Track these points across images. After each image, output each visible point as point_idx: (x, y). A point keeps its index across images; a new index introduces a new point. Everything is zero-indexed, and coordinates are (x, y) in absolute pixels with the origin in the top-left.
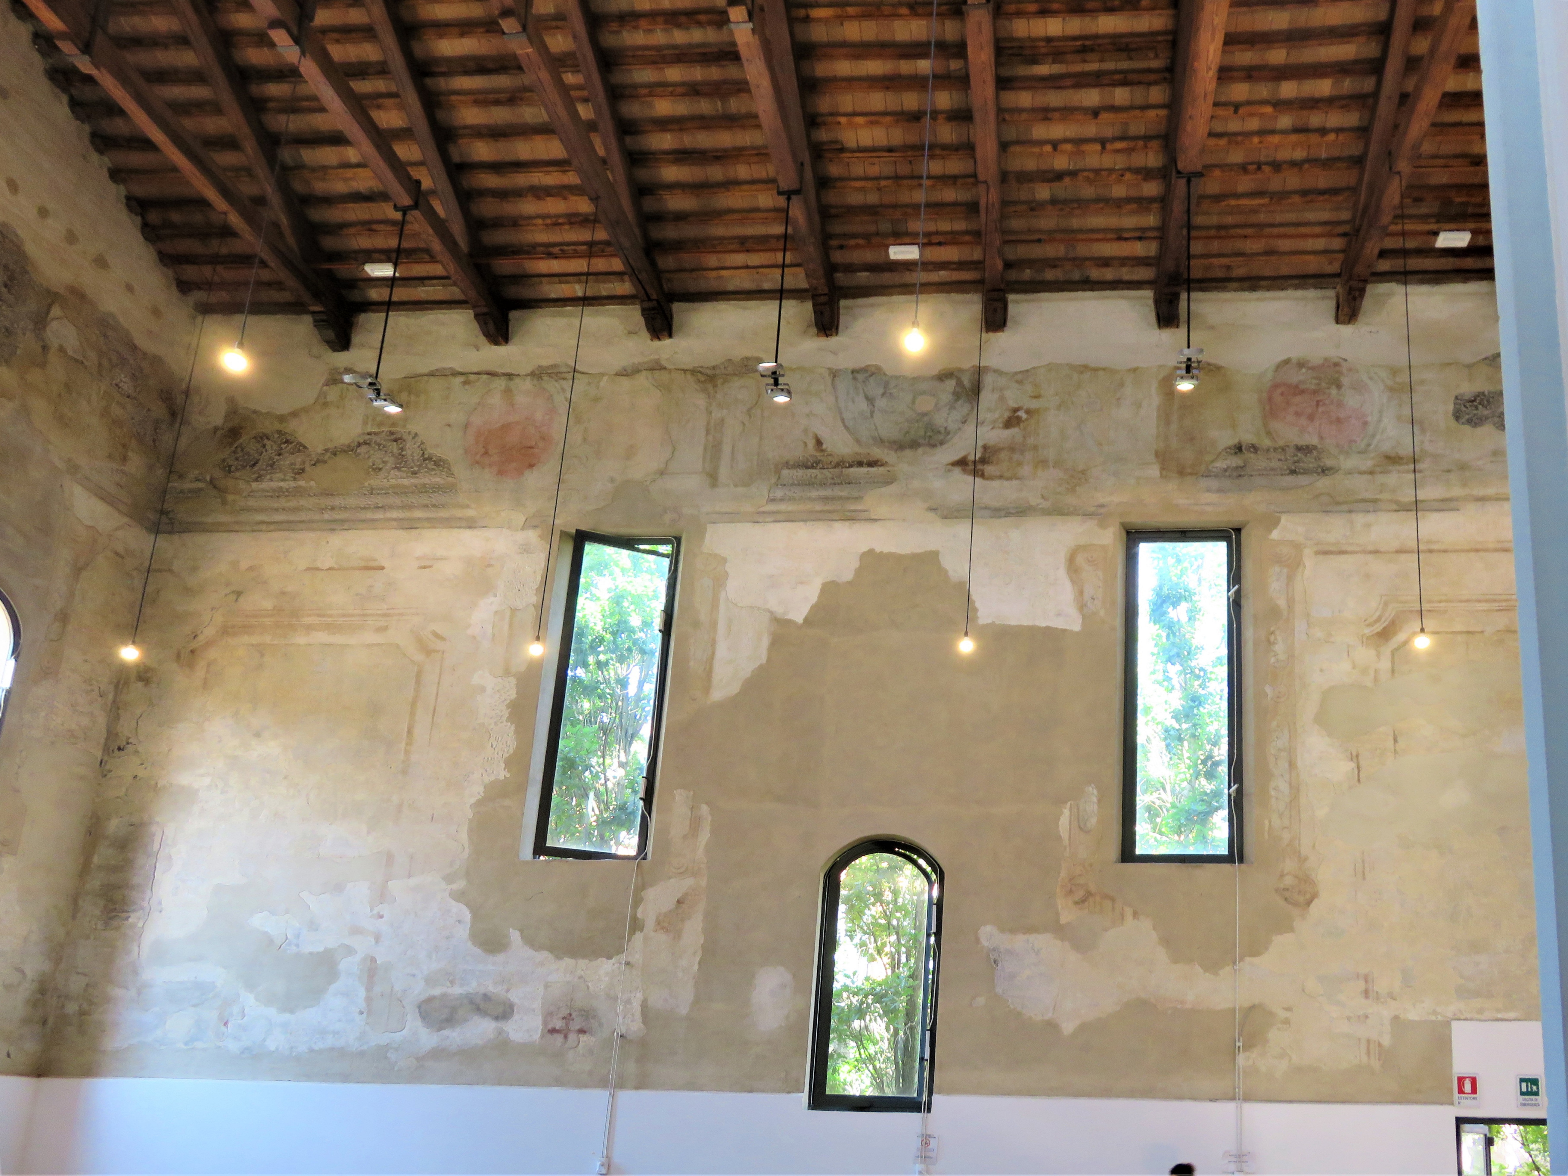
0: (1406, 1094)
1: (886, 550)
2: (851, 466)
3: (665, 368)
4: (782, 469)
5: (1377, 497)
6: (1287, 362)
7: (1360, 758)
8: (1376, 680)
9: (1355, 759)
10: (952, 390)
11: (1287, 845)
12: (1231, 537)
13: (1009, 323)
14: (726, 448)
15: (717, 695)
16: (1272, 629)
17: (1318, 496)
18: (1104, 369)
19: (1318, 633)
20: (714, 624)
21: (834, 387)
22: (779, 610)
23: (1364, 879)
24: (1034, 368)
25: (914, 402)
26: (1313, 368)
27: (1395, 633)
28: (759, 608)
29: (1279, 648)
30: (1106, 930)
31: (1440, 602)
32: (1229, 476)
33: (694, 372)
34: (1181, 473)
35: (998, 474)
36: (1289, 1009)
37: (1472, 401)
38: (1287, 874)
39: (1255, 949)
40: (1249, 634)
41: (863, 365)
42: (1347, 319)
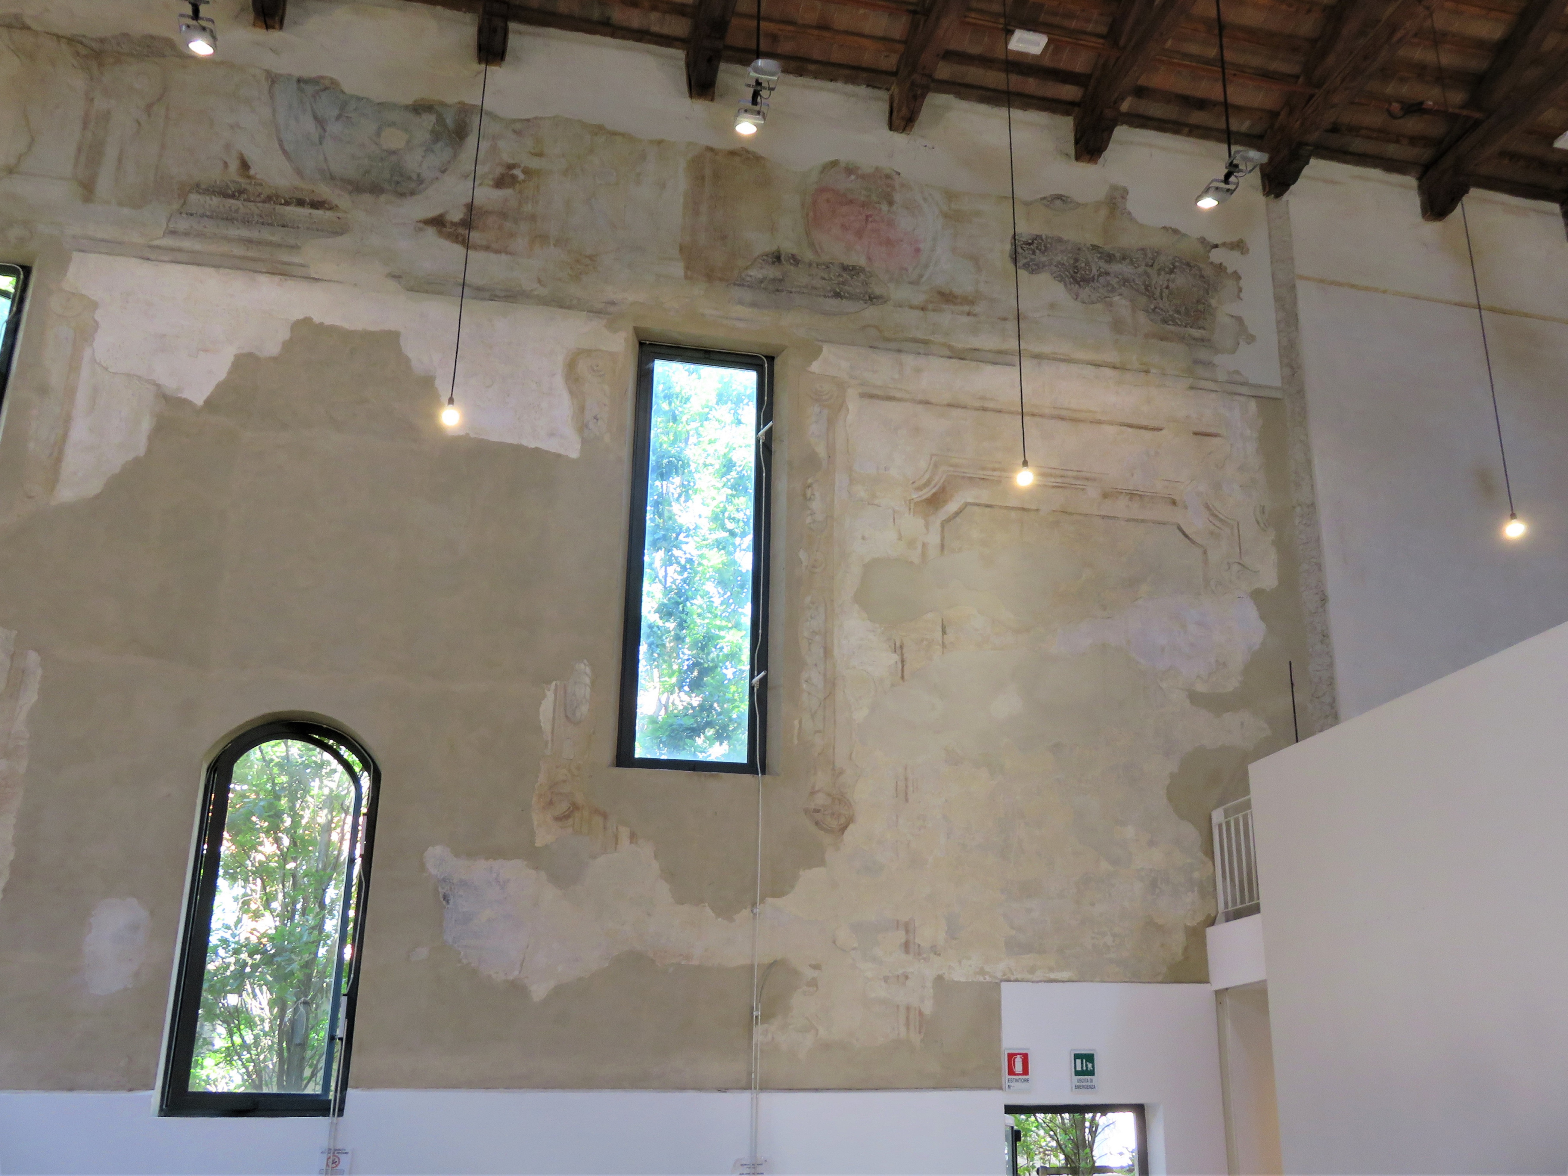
0: (950, 1079)
1: (328, 321)
2: (287, 203)
3: (29, 28)
4: (190, 192)
5: (928, 338)
6: (834, 164)
7: (905, 650)
8: (924, 555)
9: (899, 651)
10: (430, 128)
11: (819, 754)
12: (762, 366)
13: (508, 57)
14: (111, 152)
15: (66, 494)
16: (809, 481)
17: (864, 328)
18: (623, 135)
19: (861, 492)
20: (70, 392)
21: (272, 96)
22: (170, 384)
23: (907, 800)
24: (536, 118)
25: (378, 134)
26: (863, 177)
27: (945, 502)
28: (140, 378)
29: (816, 505)
30: (594, 857)
31: (994, 470)
32: (765, 289)
33: (71, 40)
34: (710, 276)
35: (484, 243)
36: (816, 967)
37: (1030, 244)
38: (818, 791)
39: (779, 886)
40: (781, 486)
41: (314, 75)
42: (903, 124)
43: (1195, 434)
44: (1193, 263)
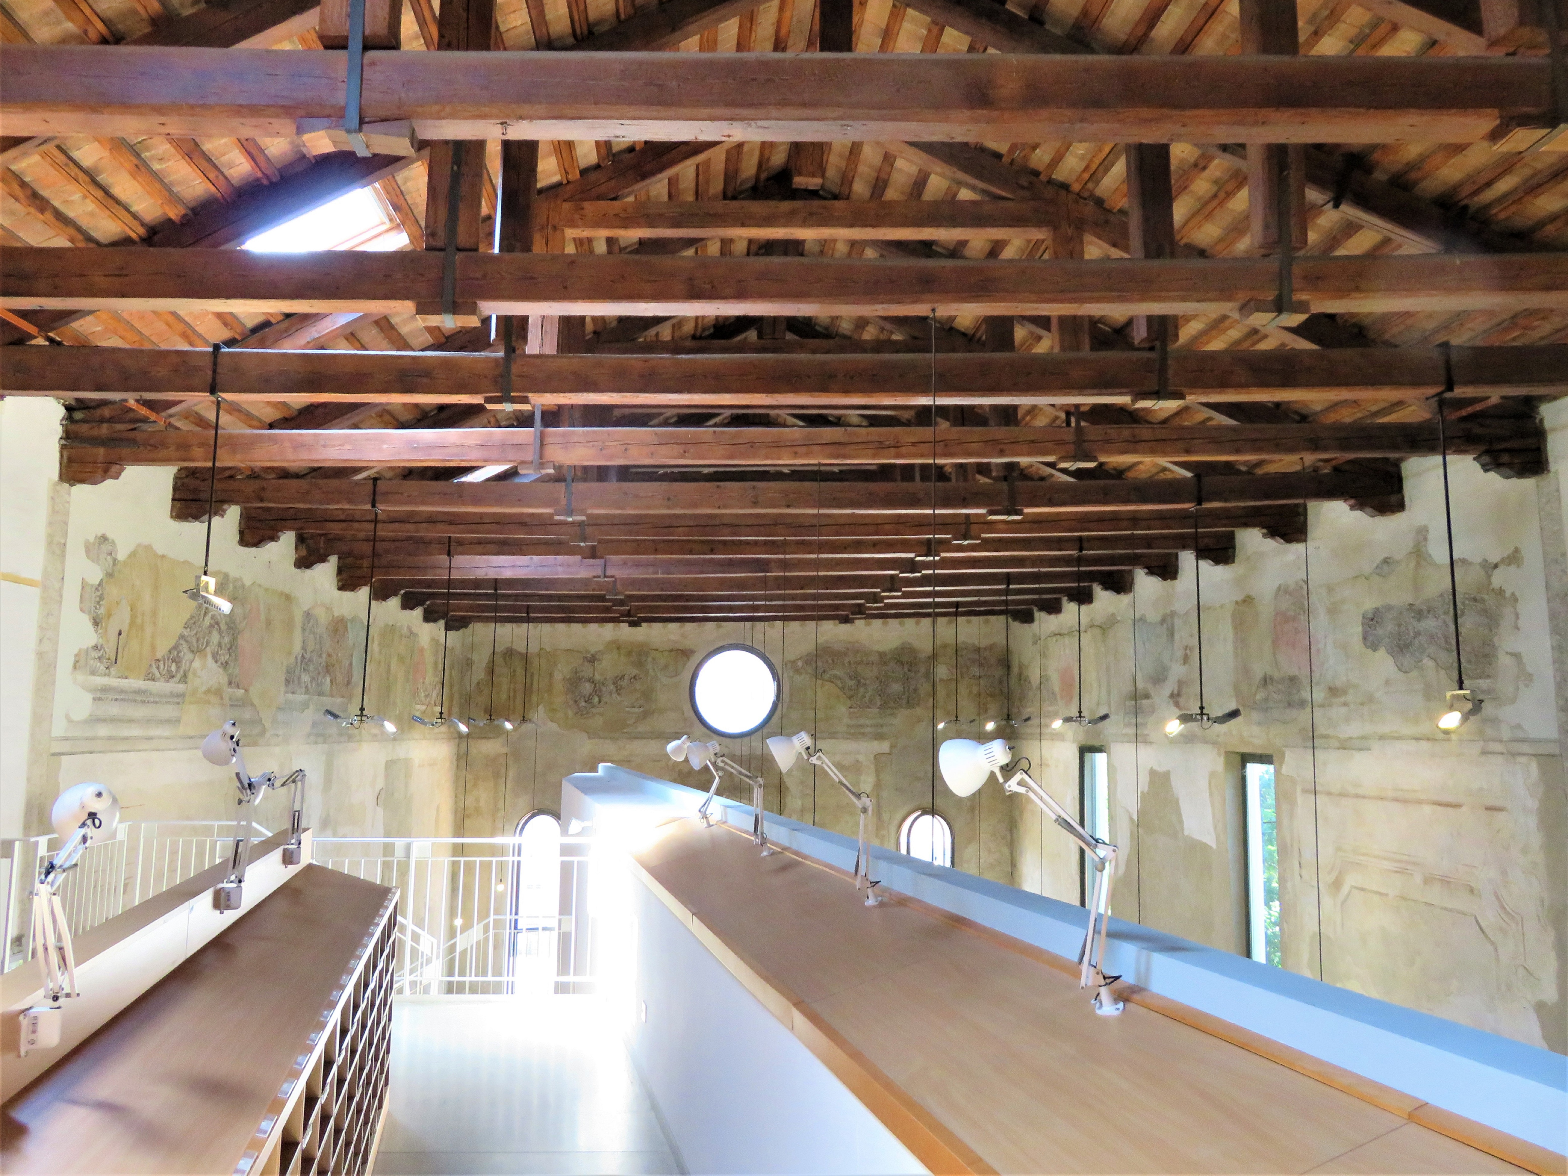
43: (1488, 809)
44: (1478, 597)
